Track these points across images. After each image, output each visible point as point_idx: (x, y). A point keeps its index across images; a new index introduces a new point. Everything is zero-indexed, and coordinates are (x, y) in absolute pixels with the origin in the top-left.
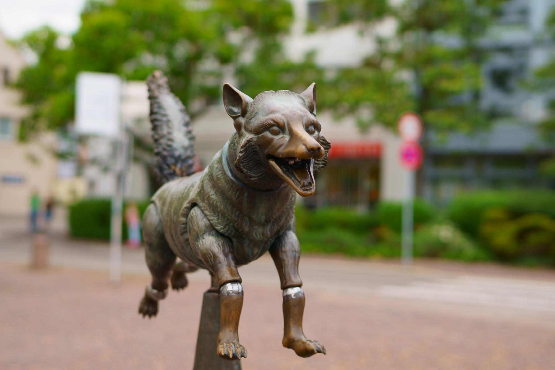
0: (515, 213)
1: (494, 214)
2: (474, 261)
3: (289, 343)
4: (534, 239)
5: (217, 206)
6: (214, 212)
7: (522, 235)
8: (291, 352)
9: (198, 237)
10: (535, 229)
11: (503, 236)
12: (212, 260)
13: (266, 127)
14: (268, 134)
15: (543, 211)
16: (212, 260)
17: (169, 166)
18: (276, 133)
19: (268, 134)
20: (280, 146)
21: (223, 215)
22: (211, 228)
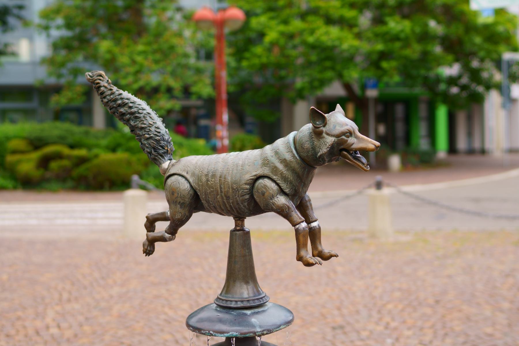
0: (36, 144)
1: (14, 144)
2: (15, 188)
3: (300, 258)
4: (54, 165)
5: (288, 178)
6: (285, 182)
7: (45, 162)
8: (300, 263)
9: (272, 197)
10: (59, 156)
11: (27, 164)
12: (287, 210)
13: (343, 134)
14: (343, 137)
15: (61, 140)
16: (287, 210)
17: (163, 147)
18: (348, 137)
19: (343, 137)
20: (353, 144)
21: (291, 183)
22: (282, 192)
